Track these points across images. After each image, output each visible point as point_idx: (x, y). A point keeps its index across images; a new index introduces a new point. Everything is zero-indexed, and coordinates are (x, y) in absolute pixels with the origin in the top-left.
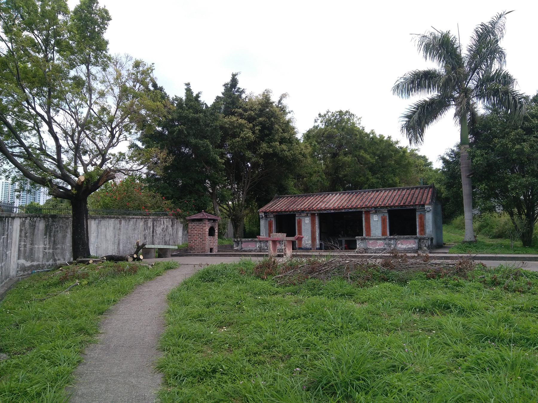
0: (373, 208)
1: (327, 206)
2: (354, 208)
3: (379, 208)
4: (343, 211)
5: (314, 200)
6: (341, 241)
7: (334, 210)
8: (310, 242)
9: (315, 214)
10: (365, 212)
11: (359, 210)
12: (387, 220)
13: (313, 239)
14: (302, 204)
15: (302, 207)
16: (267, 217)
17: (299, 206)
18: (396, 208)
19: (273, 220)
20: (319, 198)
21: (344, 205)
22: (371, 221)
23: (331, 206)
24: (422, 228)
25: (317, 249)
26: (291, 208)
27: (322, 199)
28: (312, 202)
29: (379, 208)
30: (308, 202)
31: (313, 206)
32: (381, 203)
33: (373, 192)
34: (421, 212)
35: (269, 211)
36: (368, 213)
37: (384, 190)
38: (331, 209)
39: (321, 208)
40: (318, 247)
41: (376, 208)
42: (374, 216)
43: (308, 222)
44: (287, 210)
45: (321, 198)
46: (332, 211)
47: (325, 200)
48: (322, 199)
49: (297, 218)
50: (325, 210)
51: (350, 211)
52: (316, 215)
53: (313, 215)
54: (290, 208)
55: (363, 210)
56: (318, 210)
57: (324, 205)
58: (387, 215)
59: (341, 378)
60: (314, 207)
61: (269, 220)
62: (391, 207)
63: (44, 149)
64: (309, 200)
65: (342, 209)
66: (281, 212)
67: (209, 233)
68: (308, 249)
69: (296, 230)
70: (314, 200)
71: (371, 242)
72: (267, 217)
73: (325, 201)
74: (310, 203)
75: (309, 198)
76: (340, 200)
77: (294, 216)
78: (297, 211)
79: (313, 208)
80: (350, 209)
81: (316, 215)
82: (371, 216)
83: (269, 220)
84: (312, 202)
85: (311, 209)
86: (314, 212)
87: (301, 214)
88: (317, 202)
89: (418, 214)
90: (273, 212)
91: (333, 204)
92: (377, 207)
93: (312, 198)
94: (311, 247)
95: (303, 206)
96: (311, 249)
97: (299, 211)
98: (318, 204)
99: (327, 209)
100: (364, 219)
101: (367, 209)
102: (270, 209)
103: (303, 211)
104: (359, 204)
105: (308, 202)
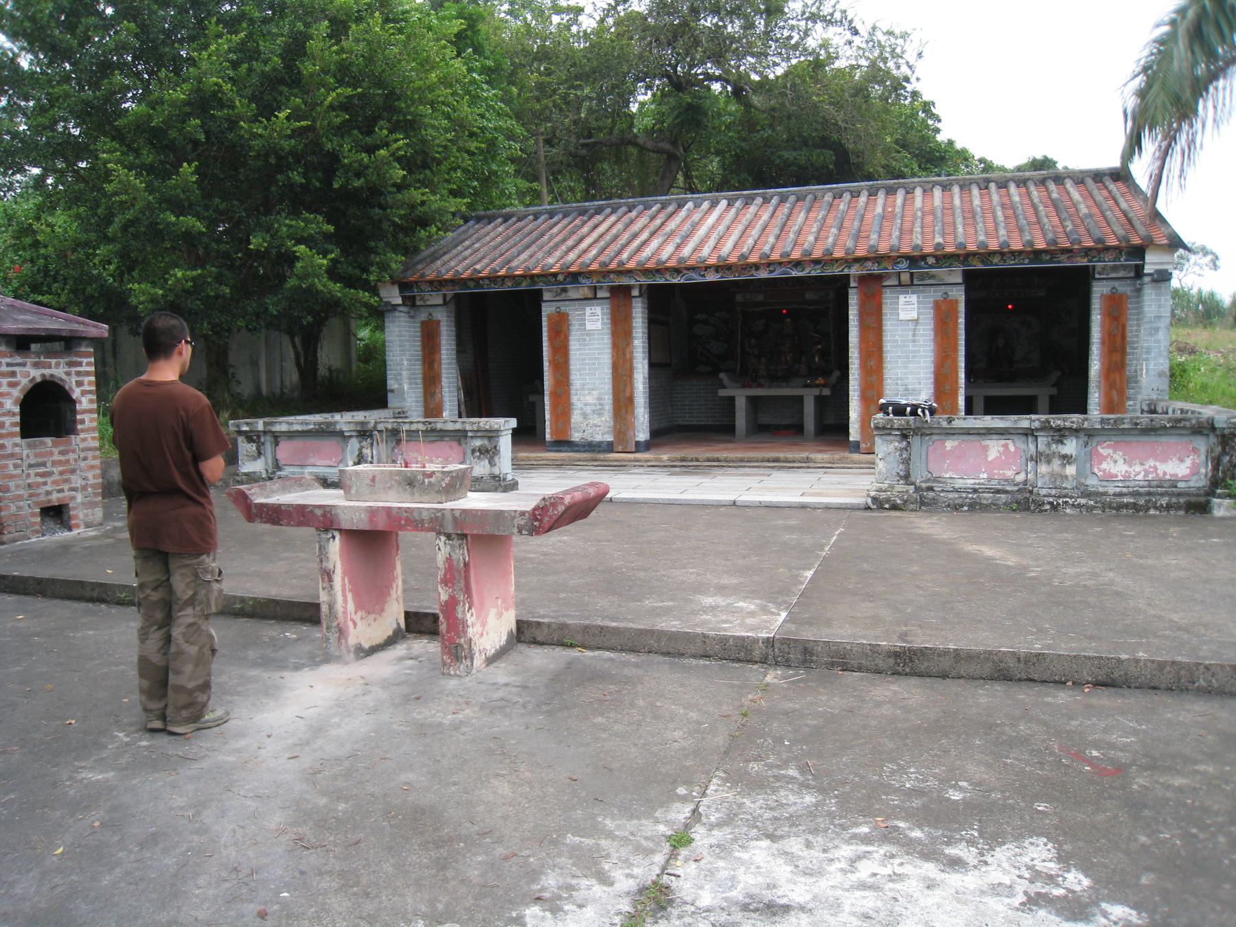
1: (686, 251)
2: (816, 262)
3: (931, 261)
4: (763, 274)
5: (620, 226)
6: (732, 399)
7: (717, 268)
8: (607, 418)
9: (628, 289)
10: (863, 279)
11: (836, 271)
13: (622, 403)
14: (570, 243)
15: (572, 256)
16: (413, 305)
17: (558, 254)
18: (1011, 264)
20: (643, 220)
21: (767, 248)
22: (888, 325)
23: (706, 251)
24: (1116, 357)
25: (641, 447)
26: (520, 265)
27: (658, 222)
28: (616, 238)
29: (931, 261)
30: (595, 235)
31: (619, 252)
34: (1116, 284)
36: (873, 284)
38: (707, 268)
39: (659, 262)
40: (643, 435)
41: (915, 260)
42: (902, 299)
43: (599, 325)
44: (502, 272)
45: (653, 218)
46: (712, 277)
47: (672, 225)
48: (658, 222)
49: (547, 310)
50: (677, 271)
51: (795, 273)
52: (635, 293)
53: (620, 295)
54: (514, 264)
55: (855, 271)
56: (646, 272)
57: (669, 249)
58: (959, 295)
60: (625, 256)
61: (423, 316)
62: (986, 255)
64: (601, 229)
65: (756, 266)
66: (477, 281)
67: (542, 296)
68: (599, 444)
69: (546, 364)
70: (620, 226)
71: (950, 444)
72: (413, 305)
73: (671, 234)
74: (608, 237)
75: (599, 218)
76: (740, 227)
77: (535, 298)
78: (549, 277)
79: (622, 264)
80: (797, 264)
81: (635, 293)
82: (888, 296)
83: (423, 316)
84: (616, 238)
85: (613, 266)
86: (625, 281)
87: (564, 290)
88: (635, 236)
89: (1099, 291)
91: (711, 242)
92: (924, 257)
93: (613, 218)
94: (609, 438)
95: (576, 251)
96: (610, 447)
97: (555, 275)
98: (644, 243)
99: (688, 269)
101: (874, 269)
103: (574, 277)
105: (595, 235)
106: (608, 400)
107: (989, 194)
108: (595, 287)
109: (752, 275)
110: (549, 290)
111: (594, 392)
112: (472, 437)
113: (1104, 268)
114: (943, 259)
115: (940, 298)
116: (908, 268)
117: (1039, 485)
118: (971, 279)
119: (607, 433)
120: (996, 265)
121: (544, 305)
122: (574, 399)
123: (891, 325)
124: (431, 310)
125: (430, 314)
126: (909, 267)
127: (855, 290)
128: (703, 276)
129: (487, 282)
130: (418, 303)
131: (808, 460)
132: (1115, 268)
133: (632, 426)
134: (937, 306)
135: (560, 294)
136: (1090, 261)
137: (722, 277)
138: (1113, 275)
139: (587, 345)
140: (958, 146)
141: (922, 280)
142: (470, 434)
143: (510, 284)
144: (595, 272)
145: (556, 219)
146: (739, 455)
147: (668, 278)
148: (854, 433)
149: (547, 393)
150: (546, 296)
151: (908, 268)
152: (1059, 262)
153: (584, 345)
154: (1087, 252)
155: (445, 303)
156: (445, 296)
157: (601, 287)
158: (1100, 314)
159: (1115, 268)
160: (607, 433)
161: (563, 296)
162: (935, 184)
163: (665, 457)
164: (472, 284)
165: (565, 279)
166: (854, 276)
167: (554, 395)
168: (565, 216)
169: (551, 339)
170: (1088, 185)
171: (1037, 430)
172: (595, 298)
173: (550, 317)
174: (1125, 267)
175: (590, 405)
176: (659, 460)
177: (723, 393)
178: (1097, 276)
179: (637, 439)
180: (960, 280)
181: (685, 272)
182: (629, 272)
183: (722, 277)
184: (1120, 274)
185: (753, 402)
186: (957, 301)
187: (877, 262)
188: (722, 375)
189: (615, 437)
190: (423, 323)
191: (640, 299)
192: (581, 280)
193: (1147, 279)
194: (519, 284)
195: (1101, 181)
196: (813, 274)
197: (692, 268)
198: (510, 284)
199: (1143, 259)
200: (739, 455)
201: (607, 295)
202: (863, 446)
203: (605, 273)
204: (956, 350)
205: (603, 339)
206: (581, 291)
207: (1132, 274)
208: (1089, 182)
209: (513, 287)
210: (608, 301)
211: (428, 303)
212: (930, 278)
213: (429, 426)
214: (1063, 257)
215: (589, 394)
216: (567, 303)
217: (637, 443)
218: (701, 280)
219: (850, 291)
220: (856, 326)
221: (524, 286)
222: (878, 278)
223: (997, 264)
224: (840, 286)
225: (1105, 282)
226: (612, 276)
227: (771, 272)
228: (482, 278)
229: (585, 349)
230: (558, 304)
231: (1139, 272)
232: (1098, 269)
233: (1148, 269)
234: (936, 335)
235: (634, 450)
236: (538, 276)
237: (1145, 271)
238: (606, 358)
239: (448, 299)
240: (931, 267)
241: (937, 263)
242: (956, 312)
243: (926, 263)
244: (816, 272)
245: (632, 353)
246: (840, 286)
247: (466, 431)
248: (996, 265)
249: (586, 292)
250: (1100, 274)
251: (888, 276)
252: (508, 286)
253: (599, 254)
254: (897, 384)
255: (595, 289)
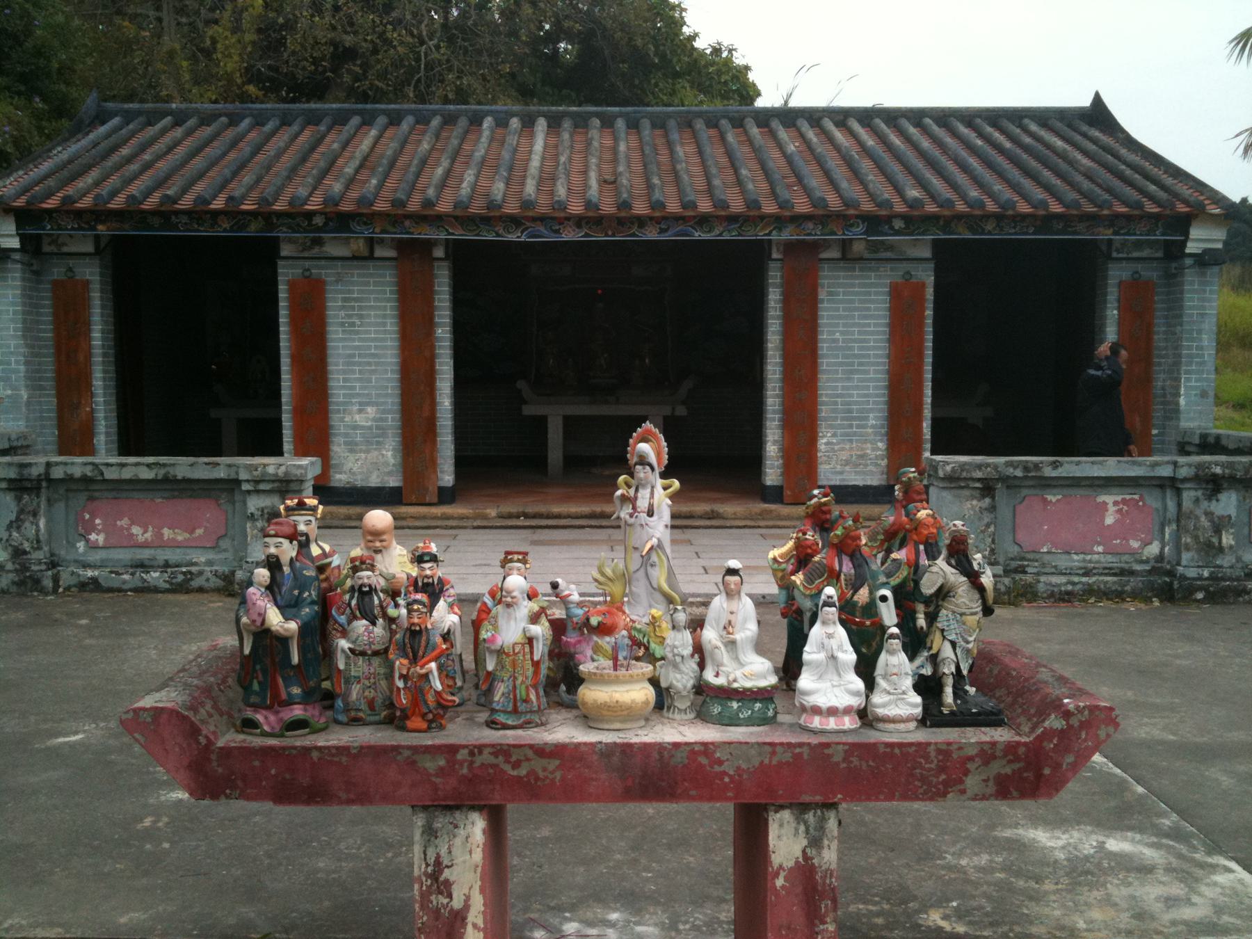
0: (860, 228)
3: (898, 224)
4: (651, 234)
6: (541, 422)
7: (579, 221)
9: (429, 245)
10: (791, 248)
12: (929, 313)
18: (1011, 234)
19: (91, 274)
25: (446, 496)
32: (303, 192)
33: (285, 122)
35: (69, 211)
37: (359, 112)
46: (570, 235)
49: (286, 274)
51: (698, 235)
52: (439, 252)
58: (927, 277)
59: (1051, 904)
61: (57, 272)
62: (974, 220)
63: (837, 568)
78: (298, 218)
81: (439, 252)
87: (318, 242)
90: (98, 215)
92: (889, 219)
97: (310, 215)
99: (534, 219)
100: (774, 297)
101: (813, 233)
102: (70, 191)
104: (114, 194)
106: (393, 420)
107: (532, 135)
108: (372, 238)
109: (634, 235)
110: (290, 241)
111: (369, 409)
112: (249, 492)
113: (1124, 243)
114: (915, 222)
115: (899, 280)
116: (866, 233)
117: (1184, 562)
118: (944, 255)
119: (390, 473)
120: (990, 233)
121: (280, 263)
122: (335, 420)
123: (829, 317)
124: (71, 262)
125: (70, 270)
126: (866, 233)
127: (778, 264)
128: (557, 232)
129: (185, 219)
130: (47, 248)
131: (712, 515)
132: (1138, 245)
133: (433, 463)
134: (896, 293)
135: (310, 248)
136: (1116, 233)
137: (587, 235)
138: (1135, 254)
139: (357, 332)
140: (739, 60)
141: (875, 252)
142: (245, 487)
143: (226, 225)
144: (381, 214)
145: (269, 127)
146: (585, 509)
147: (501, 231)
148: (772, 475)
149: (286, 408)
150: (286, 250)
151: (866, 233)
152: (1075, 233)
153: (351, 332)
154: (1114, 220)
155: (98, 252)
156: (97, 238)
157: (382, 241)
158: (1119, 309)
159: (1138, 245)
160: (390, 473)
161: (316, 251)
162: (565, 115)
163: (492, 512)
164: (156, 221)
165: (326, 224)
166: (779, 243)
167: (298, 412)
168: (177, 124)
169: (293, 321)
170: (748, 127)
171: (1185, 480)
172: (371, 257)
173: (292, 285)
174: (1151, 244)
175: (362, 427)
176: (485, 517)
177: (528, 410)
178: (1115, 255)
179: (441, 484)
180: (927, 253)
181: (528, 224)
182: (438, 220)
183: (587, 235)
184: (1145, 253)
185: (569, 421)
186: (923, 285)
187: (822, 224)
188: (521, 384)
189: (405, 479)
190: (56, 284)
191: (445, 264)
192: (354, 225)
193: (1188, 261)
194: (243, 227)
195: (716, 126)
196: (726, 237)
197: (542, 219)
198: (226, 225)
199: (1187, 234)
200: (585, 509)
201: (392, 253)
202: (787, 493)
203: (397, 217)
204: (921, 356)
205: (384, 324)
206: (354, 246)
207: (1160, 254)
208: (828, 124)
209: (231, 230)
210: (394, 263)
211: (65, 249)
212: (886, 250)
213: (162, 472)
214: (1081, 227)
215: (360, 411)
216: (323, 262)
217: (442, 490)
218: (553, 239)
219: (772, 265)
220: (778, 318)
221: (253, 229)
222: (812, 248)
223: (991, 232)
224: (759, 251)
225: (1124, 264)
226: (407, 223)
227: (662, 231)
228: (177, 213)
229: (354, 340)
230: (307, 264)
231: (1174, 252)
232: (1116, 245)
233: (1191, 248)
234: (892, 333)
235: (435, 500)
236: (280, 214)
237: (1188, 251)
238: (389, 356)
239: (102, 245)
240: (897, 233)
241: (907, 227)
242: (922, 299)
243: (892, 228)
244: (730, 235)
245: (433, 348)
246: (759, 251)
247: (237, 482)
248: (990, 233)
249: (359, 246)
250: (1118, 251)
251: (825, 245)
252: (223, 229)
253: (97, 184)
254: (836, 403)
255: (371, 243)
